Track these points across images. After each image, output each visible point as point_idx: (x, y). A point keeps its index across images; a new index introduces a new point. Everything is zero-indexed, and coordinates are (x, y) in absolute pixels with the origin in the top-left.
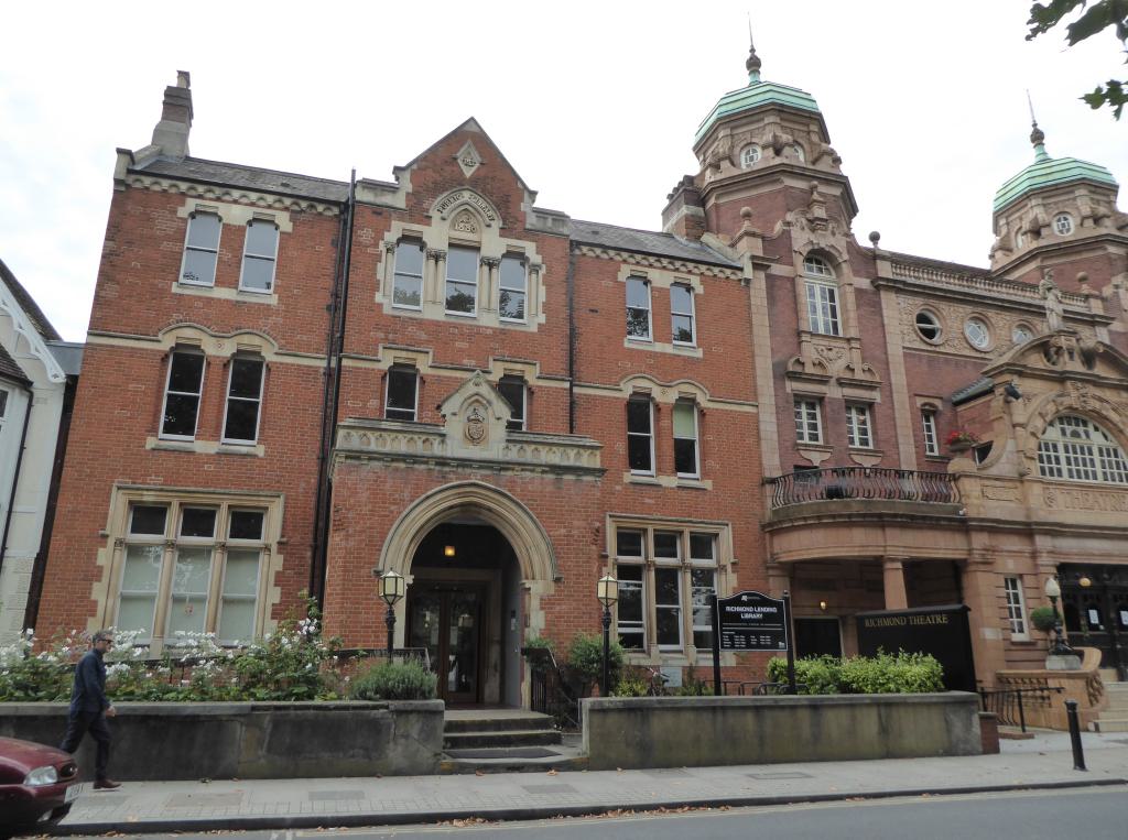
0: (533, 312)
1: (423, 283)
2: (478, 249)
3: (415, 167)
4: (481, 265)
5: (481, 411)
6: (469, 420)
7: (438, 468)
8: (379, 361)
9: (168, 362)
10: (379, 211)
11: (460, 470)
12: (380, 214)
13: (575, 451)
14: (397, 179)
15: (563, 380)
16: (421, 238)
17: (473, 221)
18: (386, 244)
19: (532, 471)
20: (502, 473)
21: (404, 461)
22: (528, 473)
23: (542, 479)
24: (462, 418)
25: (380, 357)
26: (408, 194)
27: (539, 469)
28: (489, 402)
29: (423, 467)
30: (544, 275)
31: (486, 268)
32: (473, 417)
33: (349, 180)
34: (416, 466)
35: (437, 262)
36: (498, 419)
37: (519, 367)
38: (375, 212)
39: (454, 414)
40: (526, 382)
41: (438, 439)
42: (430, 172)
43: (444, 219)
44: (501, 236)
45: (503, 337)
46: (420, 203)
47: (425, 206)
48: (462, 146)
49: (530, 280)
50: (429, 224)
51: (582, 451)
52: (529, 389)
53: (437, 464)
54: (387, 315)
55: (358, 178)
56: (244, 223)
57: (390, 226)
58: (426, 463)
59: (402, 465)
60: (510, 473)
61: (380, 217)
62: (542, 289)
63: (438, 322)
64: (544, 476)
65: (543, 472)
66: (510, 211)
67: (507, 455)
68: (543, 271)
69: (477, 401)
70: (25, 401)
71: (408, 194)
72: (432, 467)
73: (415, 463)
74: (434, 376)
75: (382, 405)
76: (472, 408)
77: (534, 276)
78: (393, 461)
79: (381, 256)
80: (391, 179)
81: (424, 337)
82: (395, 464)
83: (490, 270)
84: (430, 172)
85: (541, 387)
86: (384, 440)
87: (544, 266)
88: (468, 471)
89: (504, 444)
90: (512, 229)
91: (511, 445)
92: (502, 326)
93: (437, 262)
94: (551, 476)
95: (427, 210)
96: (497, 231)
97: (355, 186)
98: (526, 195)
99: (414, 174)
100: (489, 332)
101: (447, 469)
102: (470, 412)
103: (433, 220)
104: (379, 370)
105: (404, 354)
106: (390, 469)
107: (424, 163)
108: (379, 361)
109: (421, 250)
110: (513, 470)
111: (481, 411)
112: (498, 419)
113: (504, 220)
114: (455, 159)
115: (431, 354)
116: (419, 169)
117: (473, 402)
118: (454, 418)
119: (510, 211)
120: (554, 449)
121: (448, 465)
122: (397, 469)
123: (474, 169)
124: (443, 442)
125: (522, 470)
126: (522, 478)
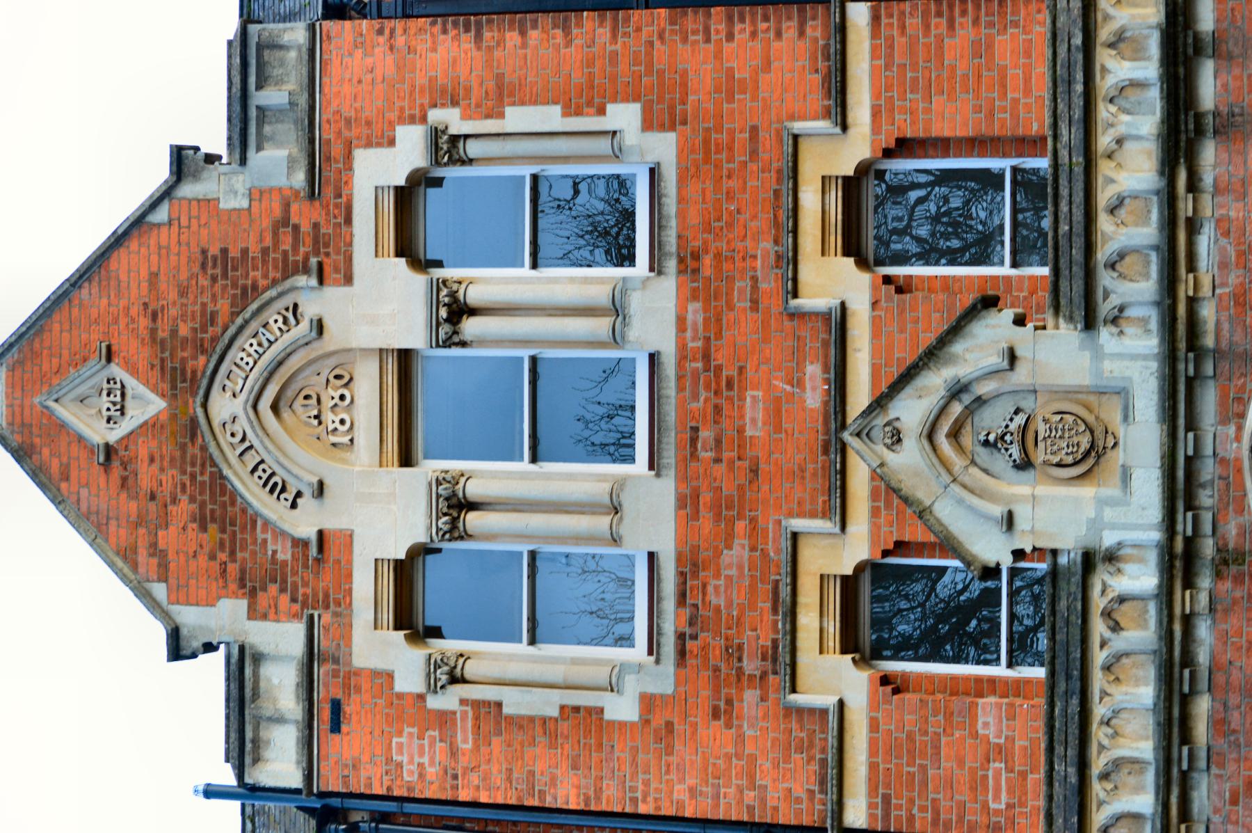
0: (603, 145)
1: (546, 548)
2: (405, 357)
3: (160, 591)
4: (463, 344)
5: (993, 419)
6: (1025, 465)
7: (1205, 582)
8: (841, 704)
9: (905, 676)
10: (327, 714)
11: (1206, 498)
12: (336, 707)
13: (1104, 56)
14: (209, 647)
15: (842, 29)
16: (399, 190)
17: (315, 383)
18: (434, 687)
19: (1193, 227)
20: (1209, 341)
21: (1186, 700)
22: (1205, 242)
23: (1217, 190)
24: (1018, 488)
25: (829, 701)
26: (253, 614)
27: (1185, 207)
28: (957, 390)
29: (1203, 630)
30: (465, 117)
31: (471, 327)
32: (1015, 450)
33: (236, 805)
34: (1203, 657)
35: (473, 506)
36: (1012, 357)
37: (810, 199)
38: (336, 727)
39: (1009, 521)
40: (864, 169)
41: (1101, 577)
42: (168, 538)
43: (320, 490)
44: (348, 280)
45: (707, 260)
46: (276, 574)
47: (285, 554)
48: (62, 426)
49: (482, 342)
50: (348, 538)
51: (1104, 33)
52: (888, 153)
53: (1189, 584)
54: (678, 683)
55: (226, 776)
56: (418, 282)
57: (376, 674)
58: (1188, 621)
59: (1203, 706)
60: (1208, 312)
61: (348, 709)
62: (517, 118)
63: (681, 502)
64: (1208, 179)
65: (1193, 186)
66: (254, 251)
67: (1144, 321)
68: (453, 120)
69: (954, 434)
70: (1034, 398)
71: (253, 614)
72: (1203, 598)
73: (1188, 660)
74: (875, 512)
75: (990, 686)
76: (983, 454)
77: (473, 149)
78: (1186, 738)
79: (477, 705)
80: (214, 665)
81: (737, 554)
82: (1201, 731)
83: (473, 312)
84: (168, 538)
85: (876, 113)
86: (1118, 763)
87: (437, 116)
88: (1208, 470)
89: (1105, 334)
90: (319, 242)
91: (1105, 308)
92: (671, 265)
93: (473, 506)
94: (1209, 153)
95: (303, 544)
96: (333, 293)
97: (248, 791)
98: (188, 190)
99: (182, 595)
100: (695, 312)
101: (1208, 548)
102: (1000, 463)
103: (331, 523)
104: (873, 705)
105: (808, 620)
106: (1221, 744)
107: (142, 556)
108: (841, 704)
109: (438, 182)
110: (1192, 301)
111: (993, 419)
112: (1012, 357)
113: (290, 269)
114: (109, 450)
115: (798, 524)
116: (163, 578)
117: (960, 448)
118: (1021, 523)
119: (254, 251)
120: (1104, 141)
121: (1191, 543)
122: (1219, 724)
123: (132, 383)
124: (1111, 557)
125: (1192, 267)
126: (1223, 265)
